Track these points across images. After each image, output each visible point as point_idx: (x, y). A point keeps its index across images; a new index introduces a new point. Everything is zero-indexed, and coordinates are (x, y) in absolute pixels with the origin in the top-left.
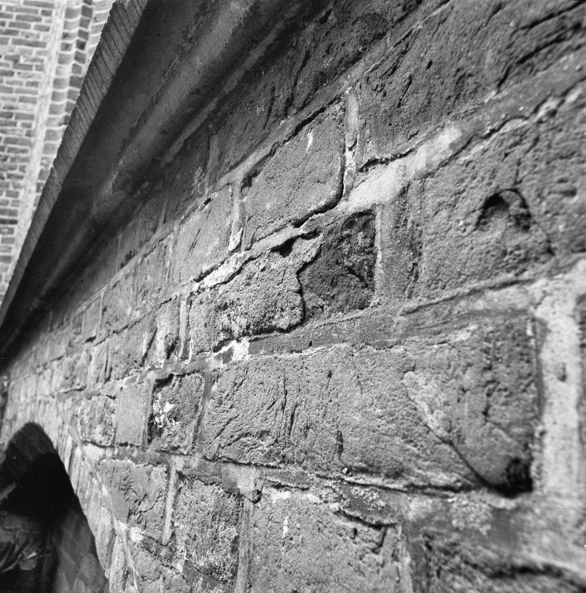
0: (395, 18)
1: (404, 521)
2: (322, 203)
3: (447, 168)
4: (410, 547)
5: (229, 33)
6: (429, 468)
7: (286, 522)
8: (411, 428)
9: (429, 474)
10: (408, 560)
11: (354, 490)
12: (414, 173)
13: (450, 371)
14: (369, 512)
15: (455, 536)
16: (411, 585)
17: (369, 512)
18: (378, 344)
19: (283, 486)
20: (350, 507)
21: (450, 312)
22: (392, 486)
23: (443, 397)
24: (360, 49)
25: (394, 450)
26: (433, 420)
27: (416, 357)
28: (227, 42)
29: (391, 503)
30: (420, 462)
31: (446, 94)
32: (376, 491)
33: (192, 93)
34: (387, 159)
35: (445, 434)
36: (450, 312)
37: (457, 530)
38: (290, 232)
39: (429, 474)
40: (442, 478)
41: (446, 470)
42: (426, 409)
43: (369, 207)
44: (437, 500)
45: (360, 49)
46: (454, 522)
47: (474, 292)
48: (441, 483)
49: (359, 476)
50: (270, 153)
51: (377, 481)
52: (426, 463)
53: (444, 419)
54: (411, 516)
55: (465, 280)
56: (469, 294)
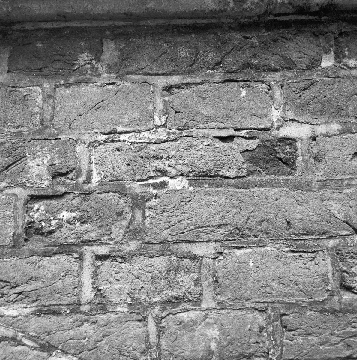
0: (301, 68)
1: (327, 248)
2: (262, 127)
3: (336, 137)
4: (330, 255)
5: (193, 9)
6: (339, 230)
7: (251, 261)
8: (331, 218)
9: (339, 232)
10: (329, 259)
11: (298, 242)
12: (319, 133)
13: (344, 201)
14: (309, 248)
15: (350, 248)
16: (331, 266)
17: (309, 248)
18: (307, 190)
19: (245, 247)
20: (297, 248)
21: (342, 183)
22: (320, 238)
23: (343, 209)
24: (278, 68)
25: (323, 226)
26: (341, 216)
27: (329, 196)
28: (187, 11)
29: (320, 244)
30: (334, 229)
31: (332, 111)
32: (311, 241)
33: (127, 14)
34: (303, 122)
35: (345, 220)
36: (342, 183)
37: (351, 246)
38: (232, 132)
39: (339, 232)
40: (344, 233)
41: (346, 230)
42: (336, 212)
43: (295, 138)
44: (341, 239)
45: (278, 68)
46: (349, 245)
47: (350, 178)
48: (345, 234)
49: (301, 237)
50: (199, 83)
51: (314, 237)
52: (338, 229)
53: (345, 215)
54: (330, 246)
55: (346, 174)
56: (349, 179)
